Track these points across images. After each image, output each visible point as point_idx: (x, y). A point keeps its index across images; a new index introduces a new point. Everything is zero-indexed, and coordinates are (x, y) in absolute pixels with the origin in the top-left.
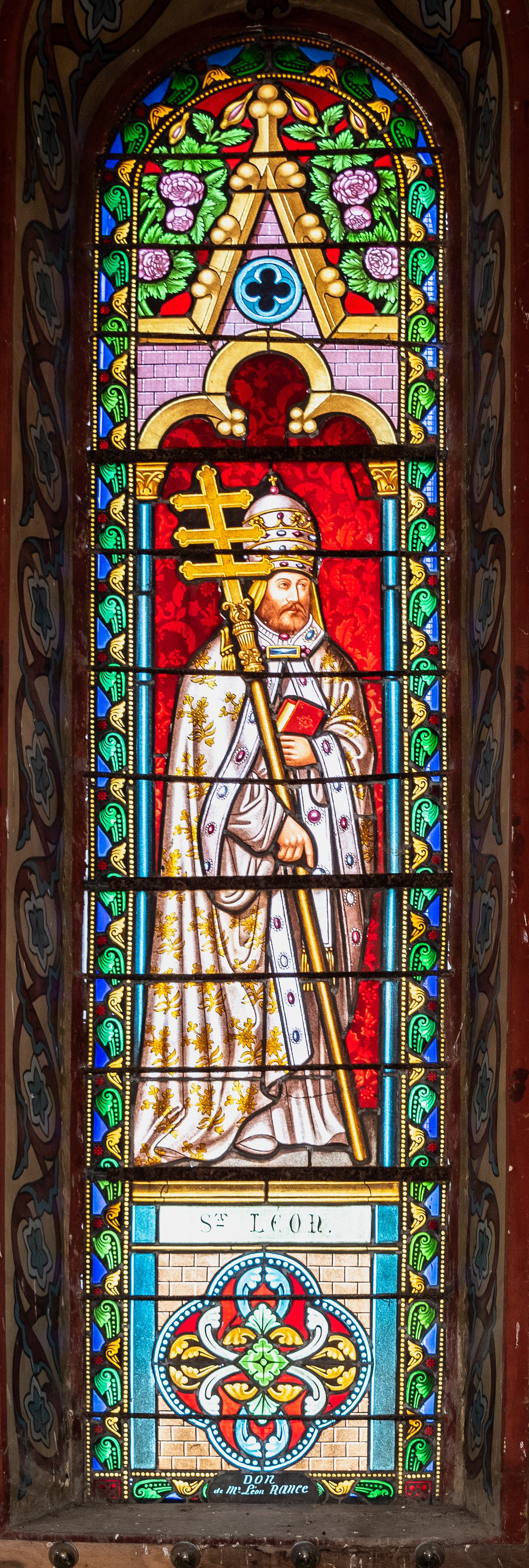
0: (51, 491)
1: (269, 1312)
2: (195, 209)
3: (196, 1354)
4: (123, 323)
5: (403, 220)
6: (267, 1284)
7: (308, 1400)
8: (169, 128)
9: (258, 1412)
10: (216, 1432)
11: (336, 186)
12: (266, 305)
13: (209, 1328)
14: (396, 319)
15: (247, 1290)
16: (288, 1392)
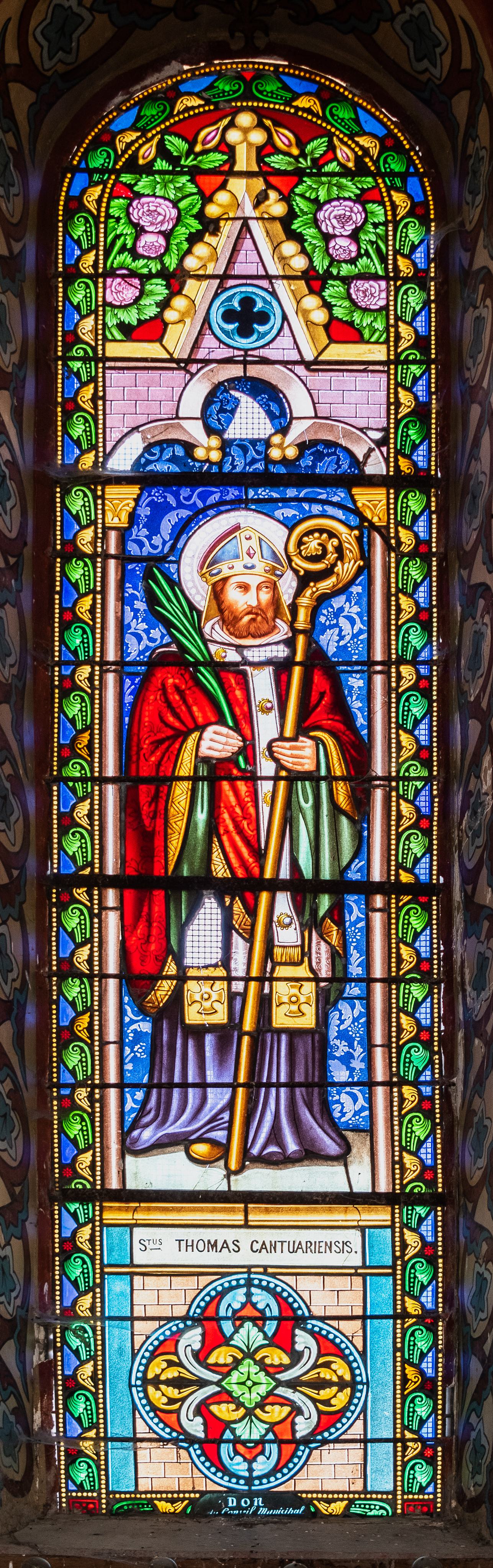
0: (10, 206)
1: (256, 1329)
2: (167, 235)
3: (176, 1374)
4: (86, 698)
5: (390, 257)
6: (254, 1305)
7: (299, 1419)
8: (138, 149)
9: (245, 1437)
10: (199, 1452)
11: (321, 215)
12: (245, 331)
13: (189, 1349)
14: (384, 347)
15: (230, 1310)
16: (277, 1413)
